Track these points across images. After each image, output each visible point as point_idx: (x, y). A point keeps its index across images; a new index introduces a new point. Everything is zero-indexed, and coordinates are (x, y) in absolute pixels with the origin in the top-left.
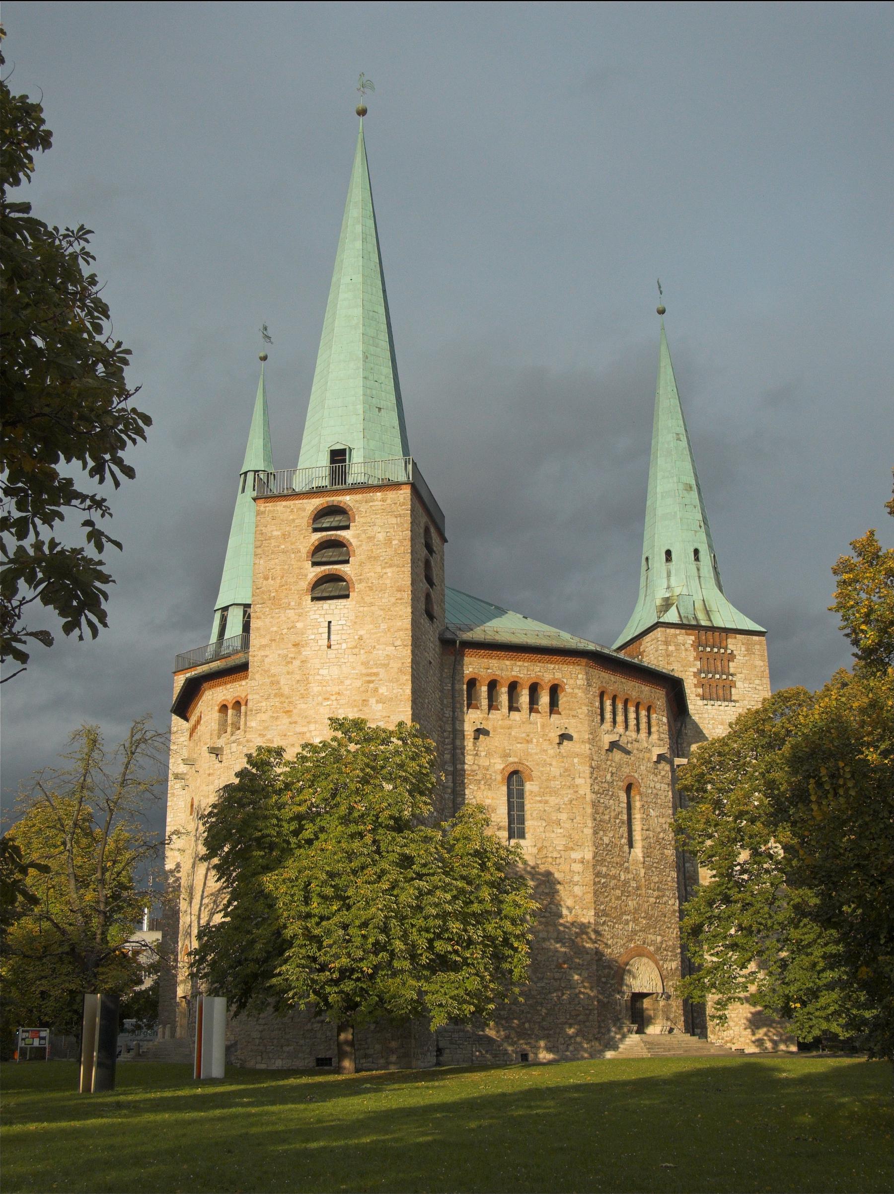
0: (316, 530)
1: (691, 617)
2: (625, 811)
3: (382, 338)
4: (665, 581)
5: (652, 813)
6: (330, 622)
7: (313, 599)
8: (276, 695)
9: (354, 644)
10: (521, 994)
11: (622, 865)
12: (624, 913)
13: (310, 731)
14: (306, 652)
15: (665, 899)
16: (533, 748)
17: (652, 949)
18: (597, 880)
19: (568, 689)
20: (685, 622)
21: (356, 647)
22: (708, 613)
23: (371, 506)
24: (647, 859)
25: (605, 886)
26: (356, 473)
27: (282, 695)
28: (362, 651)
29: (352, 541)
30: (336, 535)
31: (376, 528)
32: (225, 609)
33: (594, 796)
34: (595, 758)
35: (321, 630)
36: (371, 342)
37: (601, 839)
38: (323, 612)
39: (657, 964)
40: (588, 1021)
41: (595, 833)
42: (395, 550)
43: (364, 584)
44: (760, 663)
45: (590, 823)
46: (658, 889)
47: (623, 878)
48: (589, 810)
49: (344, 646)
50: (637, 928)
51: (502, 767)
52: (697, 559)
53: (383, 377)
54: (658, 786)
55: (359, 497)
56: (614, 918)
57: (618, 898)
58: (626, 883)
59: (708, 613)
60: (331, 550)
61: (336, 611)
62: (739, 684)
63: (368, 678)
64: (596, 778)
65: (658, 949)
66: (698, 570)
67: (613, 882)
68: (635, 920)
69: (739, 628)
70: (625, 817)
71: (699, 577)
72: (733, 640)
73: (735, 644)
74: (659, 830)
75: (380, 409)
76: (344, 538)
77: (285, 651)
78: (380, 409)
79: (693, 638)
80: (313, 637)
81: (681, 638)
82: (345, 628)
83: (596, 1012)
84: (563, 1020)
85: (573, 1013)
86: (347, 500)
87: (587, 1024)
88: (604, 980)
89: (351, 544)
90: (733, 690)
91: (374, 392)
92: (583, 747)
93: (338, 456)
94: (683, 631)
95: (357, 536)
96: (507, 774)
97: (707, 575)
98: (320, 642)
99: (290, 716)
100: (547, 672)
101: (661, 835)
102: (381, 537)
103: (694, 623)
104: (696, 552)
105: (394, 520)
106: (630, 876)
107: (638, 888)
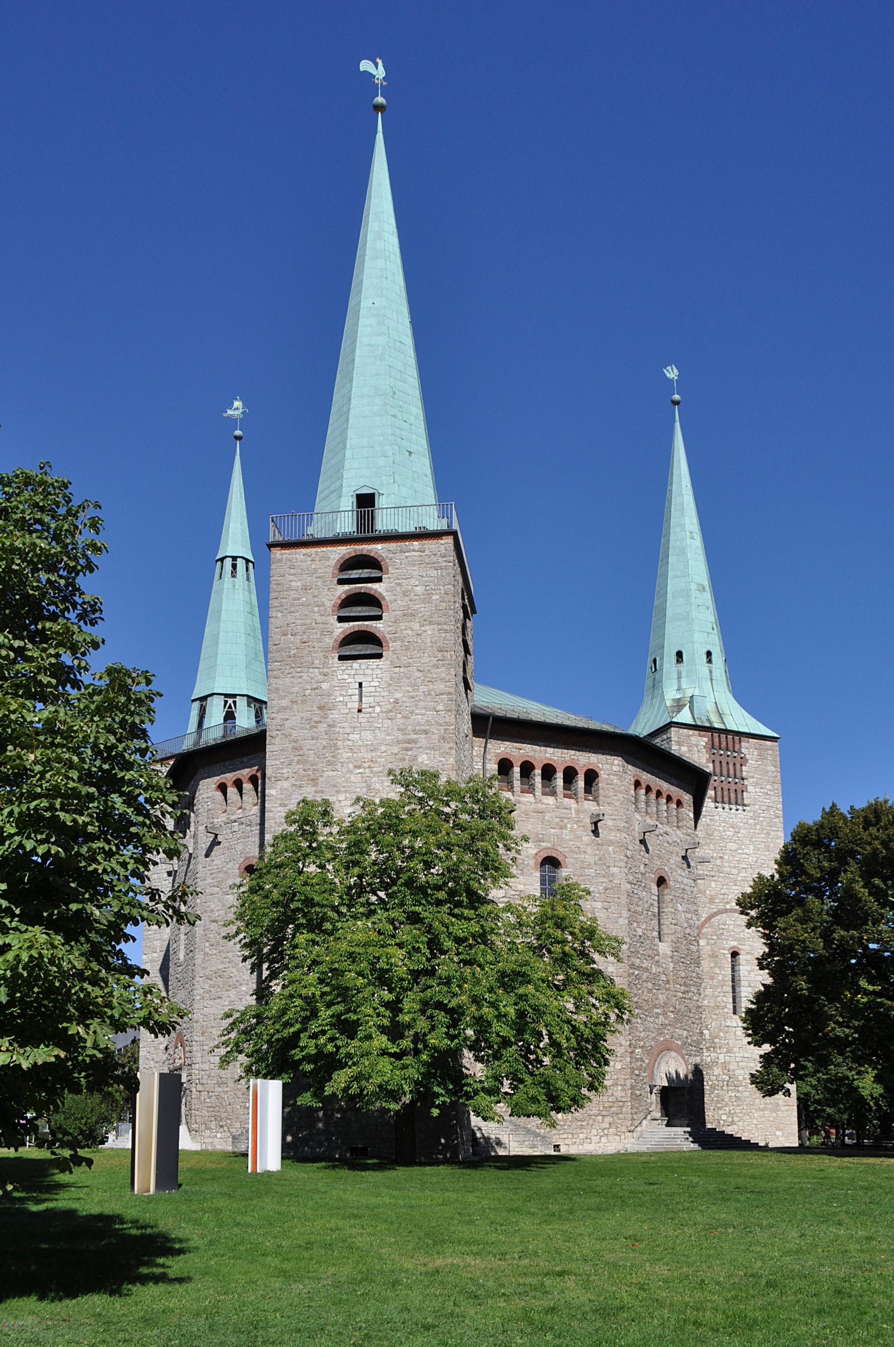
0: (341, 582)
1: (704, 719)
2: (656, 904)
3: (410, 373)
4: (675, 682)
5: (680, 908)
6: (360, 684)
7: (341, 658)
8: (298, 762)
9: (389, 707)
10: (777, 1058)
11: (653, 958)
12: (655, 1006)
13: (340, 801)
14: (334, 715)
15: (691, 994)
16: (566, 834)
17: (679, 1043)
18: (631, 971)
19: (603, 775)
20: (699, 723)
21: (391, 711)
22: (720, 715)
23: (406, 557)
24: (675, 954)
25: (637, 977)
26: (384, 522)
27: (306, 762)
28: (399, 716)
29: (385, 594)
30: (367, 588)
31: (412, 581)
32: (204, 699)
33: (629, 886)
34: (630, 847)
35: (350, 692)
36: (399, 377)
37: (635, 930)
38: (353, 672)
39: (683, 1058)
40: (621, 1113)
41: (630, 924)
42: (436, 606)
43: (399, 643)
44: (773, 769)
45: (625, 914)
46: (685, 985)
47: (654, 971)
48: (624, 900)
49: (378, 709)
50: (667, 1022)
51: (534, 851)
52: (710, 661)
53: (413, 418)
54: (686, 881)
55: (392, 546)
56: (646, 1011)
57: (650, 991)
58: (656, 976)
59: (720, 715)
60: (362, 602)
61: (368, 672)
62: (750, 788)
63: (405, 745)
64: (630, 868)
65: (684, 1044)
66: (711, 672)
67: (646, 974)
68: (664, 1014)
69: (752, 732)
70: (656, 910)
71: (711, 680)
72: (746, 744)
73: (748, 748)
74: (686, 925)
75: (410, 453)
76: (376, 591)
77: (308, 714)
78: (410, 453)
79: (706, 739)
80: (341, 699)
81: (694, 740)
82: (378, 690)
83: (629, 1104)
84: (595, 1112)
85: (607, 1105)
86: (378, 549)
87: (620, 1116)
88: (637, 1072)
89: (384, 598)
90: (745, 793)
91: (404, 433)
92: (618, 835)
93: (366, 501)
94: (697, 732)
95: (391, 590)
96: (540, 860)
97: (719, 678)
98: (349, 705)
99: (316, 785)
100: (583, 760)
101: (688, 931)
102: (419, 589)
103: (707, 725)
104: (709, 654)
105: (434, 573)
106: (661, 970)
107: (668, 982)
